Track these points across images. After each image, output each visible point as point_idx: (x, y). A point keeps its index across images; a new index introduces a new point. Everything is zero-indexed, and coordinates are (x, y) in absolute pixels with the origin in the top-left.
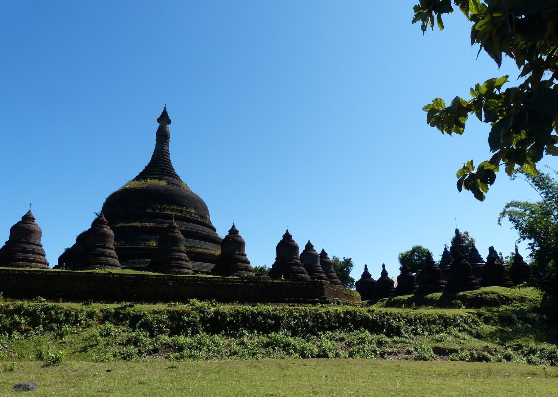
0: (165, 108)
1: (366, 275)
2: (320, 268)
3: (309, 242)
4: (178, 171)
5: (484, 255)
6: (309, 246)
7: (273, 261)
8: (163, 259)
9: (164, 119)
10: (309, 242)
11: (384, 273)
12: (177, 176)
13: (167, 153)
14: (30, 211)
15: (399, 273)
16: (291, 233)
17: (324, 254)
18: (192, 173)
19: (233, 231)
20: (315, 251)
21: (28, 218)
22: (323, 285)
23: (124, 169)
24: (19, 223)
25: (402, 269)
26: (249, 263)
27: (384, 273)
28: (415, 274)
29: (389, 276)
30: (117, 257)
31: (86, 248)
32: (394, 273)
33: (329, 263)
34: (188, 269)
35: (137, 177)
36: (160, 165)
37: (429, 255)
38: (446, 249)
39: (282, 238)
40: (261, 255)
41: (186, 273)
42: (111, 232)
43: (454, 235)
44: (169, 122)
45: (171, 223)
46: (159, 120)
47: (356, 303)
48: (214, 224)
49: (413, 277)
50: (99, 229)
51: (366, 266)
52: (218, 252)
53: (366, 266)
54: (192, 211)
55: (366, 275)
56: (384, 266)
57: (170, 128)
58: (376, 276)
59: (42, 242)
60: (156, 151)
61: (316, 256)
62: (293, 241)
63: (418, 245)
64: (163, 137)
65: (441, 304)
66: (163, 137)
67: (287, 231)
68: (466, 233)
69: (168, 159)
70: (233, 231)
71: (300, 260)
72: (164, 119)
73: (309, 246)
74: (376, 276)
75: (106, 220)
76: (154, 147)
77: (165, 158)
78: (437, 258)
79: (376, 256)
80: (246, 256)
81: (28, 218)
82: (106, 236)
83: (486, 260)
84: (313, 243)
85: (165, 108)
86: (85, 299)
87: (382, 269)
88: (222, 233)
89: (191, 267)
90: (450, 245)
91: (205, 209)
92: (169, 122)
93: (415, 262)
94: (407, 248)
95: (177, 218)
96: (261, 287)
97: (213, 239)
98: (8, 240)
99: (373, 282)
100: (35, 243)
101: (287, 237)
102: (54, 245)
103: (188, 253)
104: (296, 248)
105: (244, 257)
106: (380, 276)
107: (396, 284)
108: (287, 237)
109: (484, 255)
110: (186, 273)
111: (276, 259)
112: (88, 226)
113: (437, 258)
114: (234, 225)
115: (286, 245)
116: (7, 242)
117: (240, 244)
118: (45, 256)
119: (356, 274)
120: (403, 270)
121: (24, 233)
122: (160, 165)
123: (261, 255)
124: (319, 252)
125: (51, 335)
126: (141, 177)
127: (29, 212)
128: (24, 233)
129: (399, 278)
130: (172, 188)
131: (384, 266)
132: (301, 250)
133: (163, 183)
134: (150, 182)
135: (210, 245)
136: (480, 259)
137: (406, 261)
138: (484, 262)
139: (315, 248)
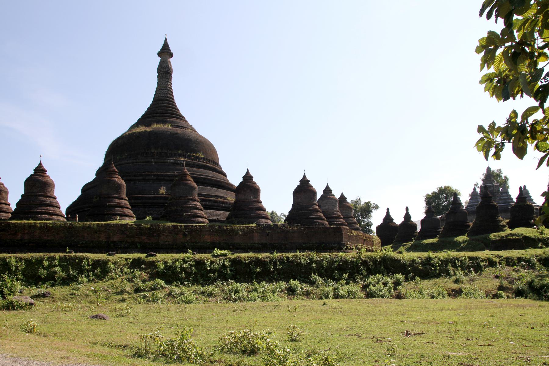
0: (166, 39)
1: (388, 219)
2: (339, 214)
3: (327, 186)
4: (183, 112)
5: (514, 194)
6: (327, 191)
7: (290, 207)
8: (175, 208)
9: (165, 52)
10: (327, 186)
11: (407, 217)
12: (182, 117)
13: (169, 92)
14: (40, 163)
15: (423, 216)
16: (308, 177)
17: (343, 198)
18: (197, 112)
19: (248, 178)
20: (334, 195)
21: (40, 170)
22: (342, 231)
23: (126, 111)
24: (31, 175)
25: (428, 212)
26: (264, 210)
27: (407, 217)
28: (440, 217)
29: (412, 219)
30: (130, 207)
31: (94, 199)
32: (418, 216)
33: (350, 208)
34: (203, 217)
35: (139, 120)
36: (163, 106)
37: (455, 195)
38: (475, 189)
39: (299, 183)
40: (277, 202)
41: (201, 222)
42: (123, 182)
43: (485, 172)
44: (171, 55)
45: (182, 170)
46: (159, 54)
47: (375, 248)
48: (224, 169)
49: (438, 219)
50: (110, 180)
51: (388, 209)
52: (231, 198)
53: (388, 209)
54: (196, 153)
55: (388, 219)
56: (407, 209)
57: (173, 61)
58: (398, 220)
59: (56, 194)
60: (158, 90)
61: (335, 200)
62: (311, 186)
63: (443, 185)
64: (165, 73)
65: (470, 247)
66: (165, 73)
67: (304, 175)
68: (499, 170)
69: (171, 98)
70: (248, 178)
71: (318, 206)
72: (165, 52)
73: (327, 191)
74: (398, 220)
75: (116, 170)
76: (156, 85)
77: (168, 97)
78: (464, 199)
79: (401, 199)
80: (261, 203)
81: (40, 170)
82: (119, 186)
83: (515, 200)
84: (331, 187)
85: (166, 39)
86: (110, 248)
87: (405, 212)
88: (235, 180)
89: (205, 215)
90: (481, 183)
91: (213, 152)
92: (171, 55)
93: (441, 202)
94: (433, 189)
95: (188, 165)
96: (275, 236)
97: (227, 187)
98: (23, 193)
99: (395, 227)
100: (50, 195)
101: (305, 182)
102: (65, 195)
103: (202, 201)
104: (314, 193)
105: (259, 205)
106: (403, 220)
107: (419, 229)
108: (305, 182)
109: (514, 194)
110: (201, 222)
111: (293, 205)
112: (91, 177)
113: (464, 199)
114: (248, 171)
115: (304, 190)
116: (22, 196)
117: (256, 191)
118: (60, 208)
119: (376, 219)
120: (428, 212)
121: (38, 184)
122: (163, 106)
123: (277, 202)
124: (337, 196)
125: (501, 123)
126: (145, 120)
127: (40, 163)
128: (38, 184)
129: (423, 222)
130: (179, 131)
131: (407, 209)
132: (319, 194)
133: (168, 127)
134: (156, 126)
135: (221, 193)
136: (509, 198)
137: (433, 201)
138: (513, 202)
139: (333, 193)
